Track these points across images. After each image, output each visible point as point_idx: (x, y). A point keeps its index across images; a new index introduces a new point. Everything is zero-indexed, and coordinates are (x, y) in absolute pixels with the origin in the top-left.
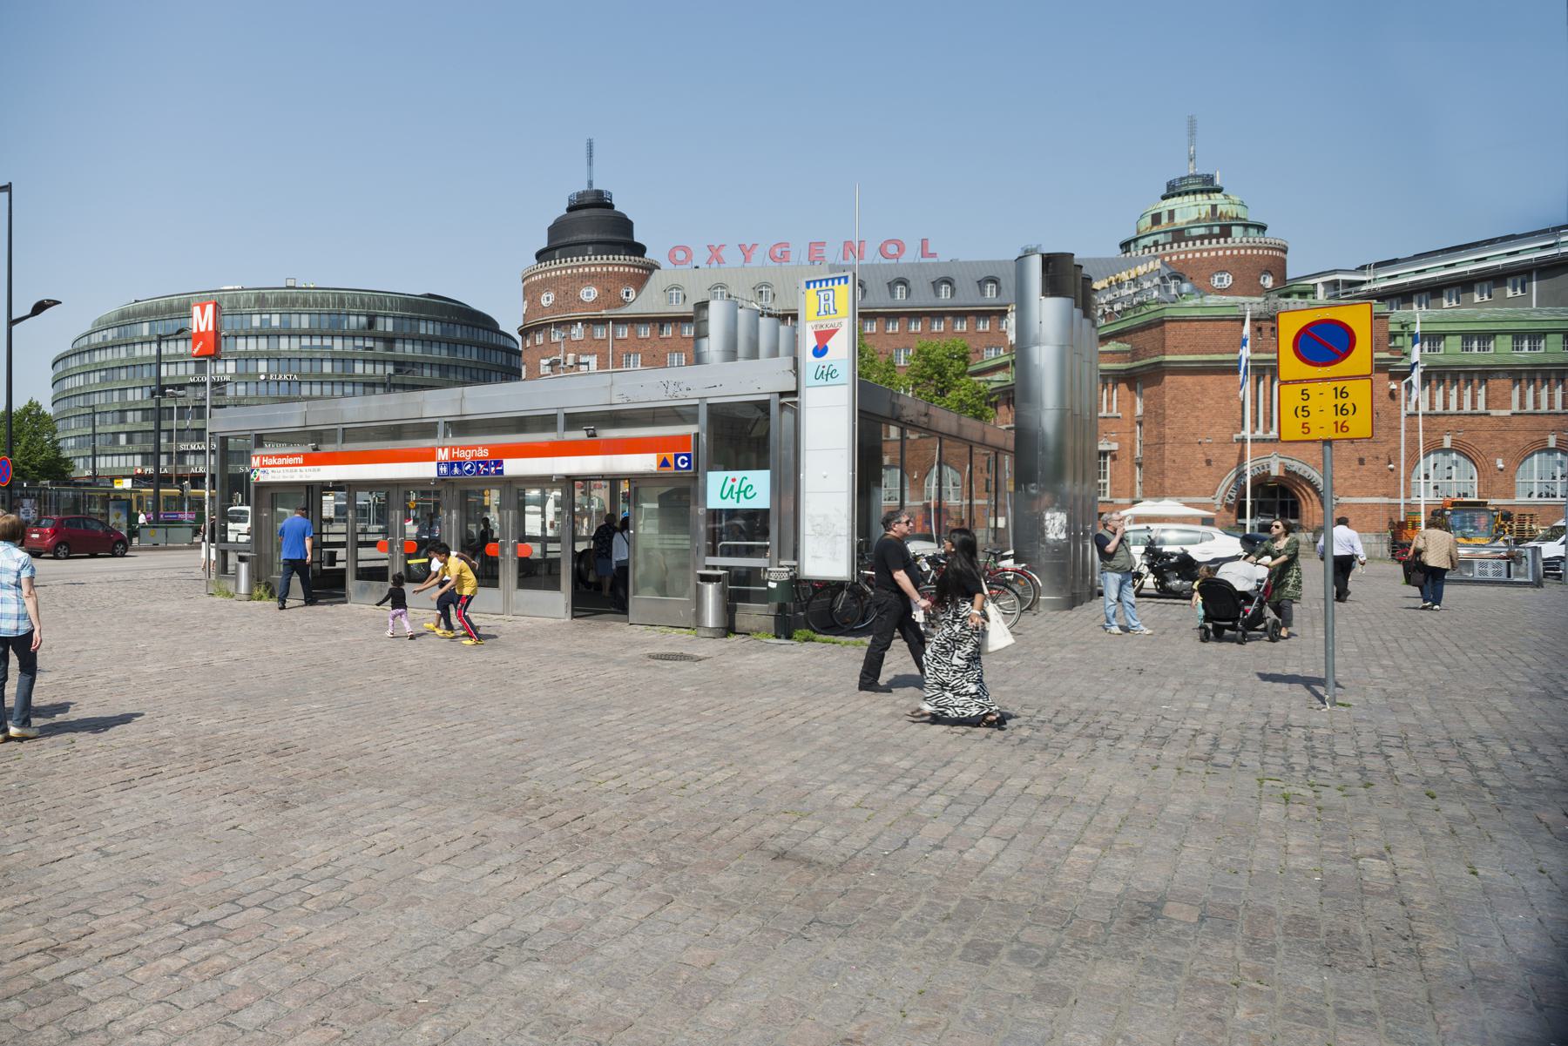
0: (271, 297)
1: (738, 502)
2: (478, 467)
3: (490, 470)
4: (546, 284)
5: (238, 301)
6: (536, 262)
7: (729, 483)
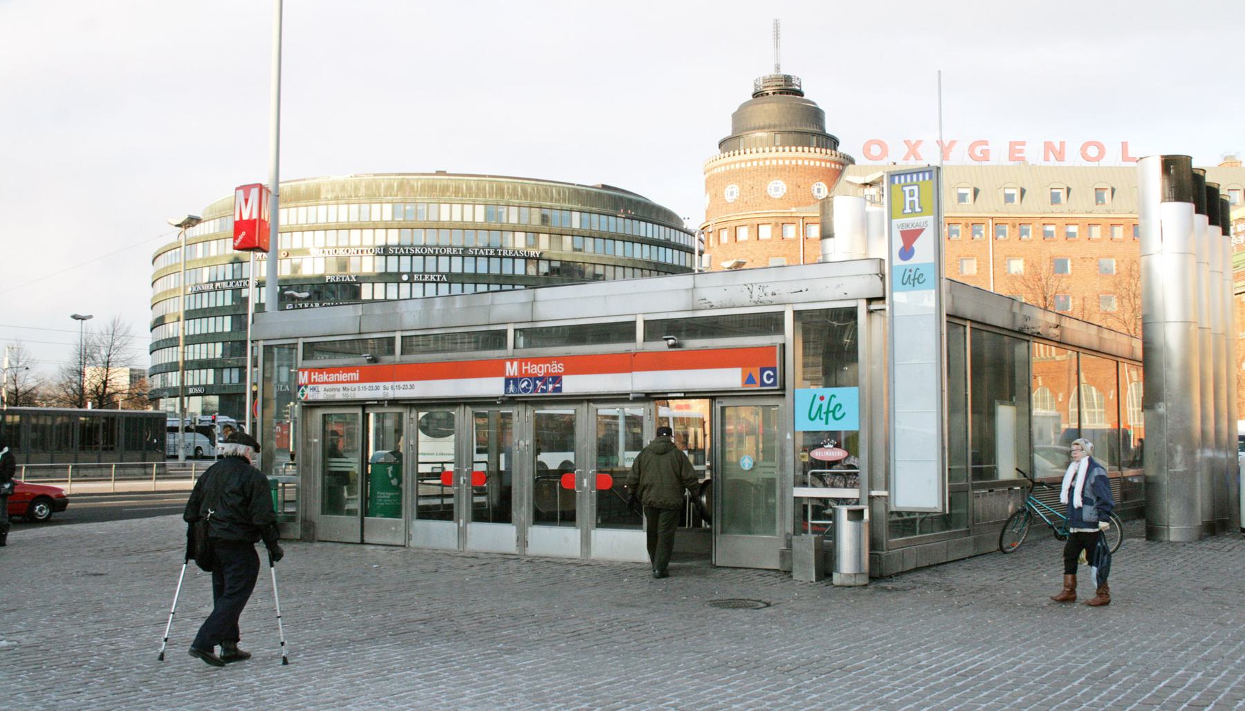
0: (417, 183)
1: (827, 423)
2: (535, 385)
3: (547, 388)
4: (732, 176)
5: (378, 187)
6: (719, 151)
7: (817, 402)
